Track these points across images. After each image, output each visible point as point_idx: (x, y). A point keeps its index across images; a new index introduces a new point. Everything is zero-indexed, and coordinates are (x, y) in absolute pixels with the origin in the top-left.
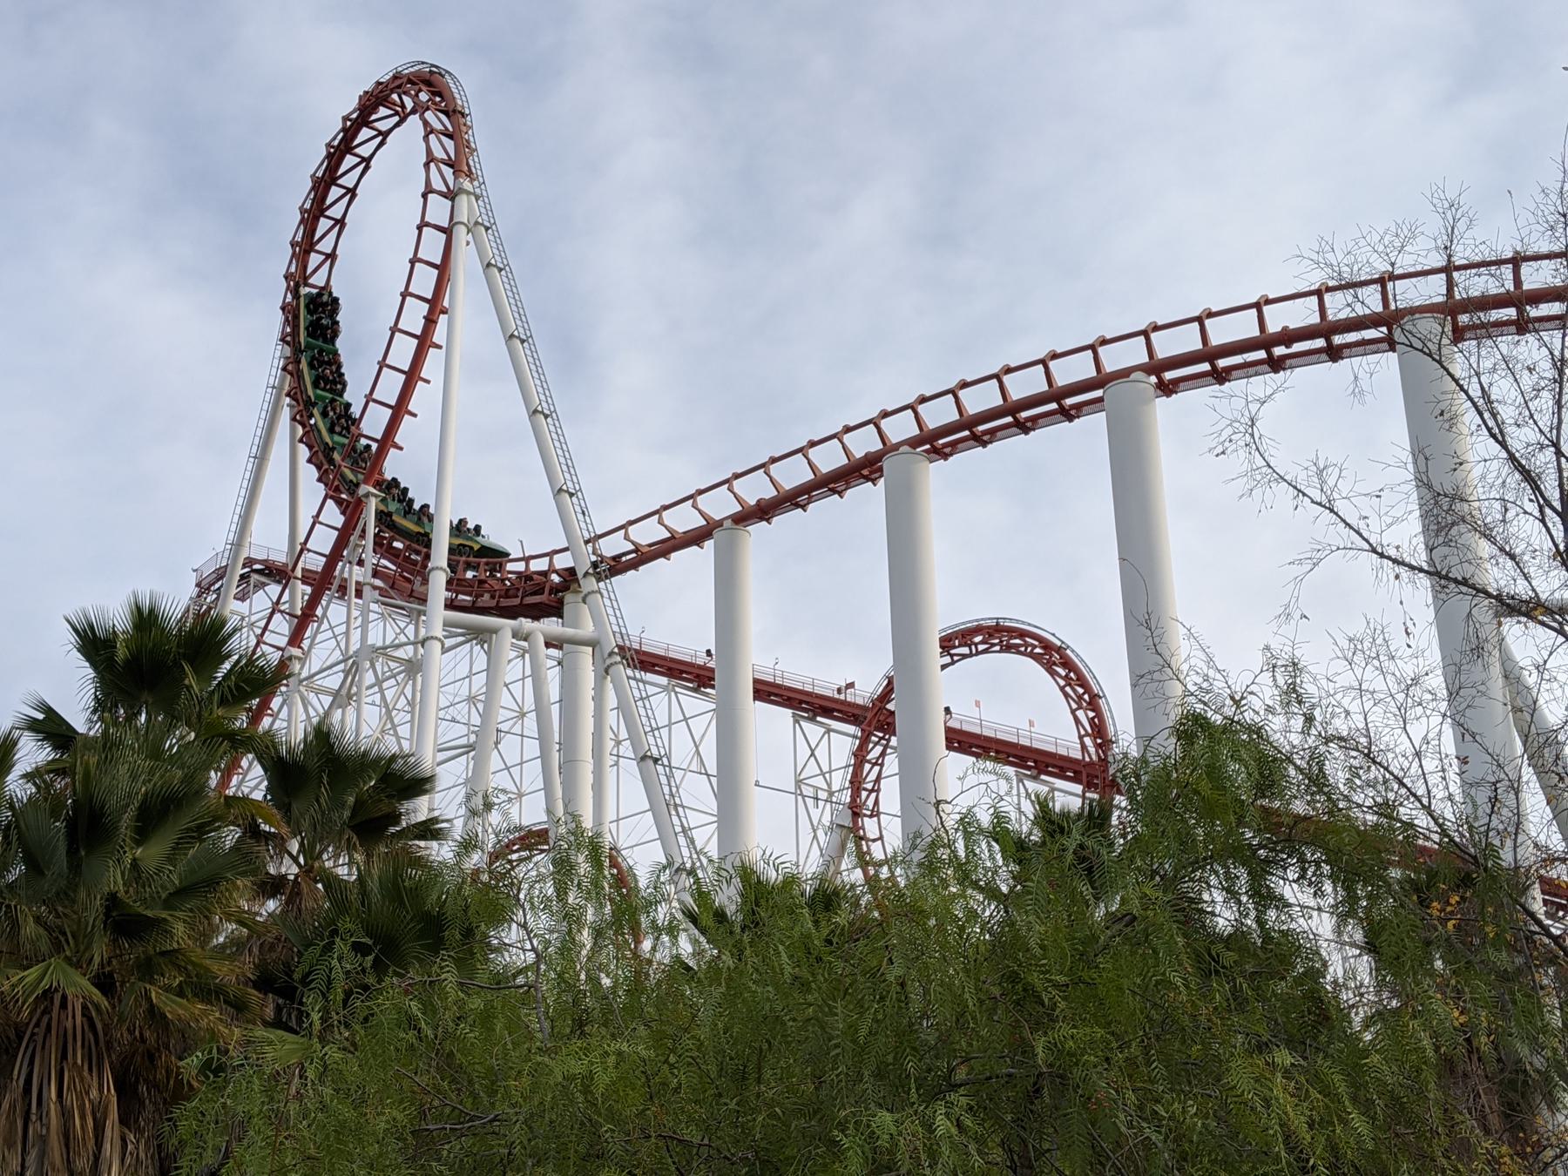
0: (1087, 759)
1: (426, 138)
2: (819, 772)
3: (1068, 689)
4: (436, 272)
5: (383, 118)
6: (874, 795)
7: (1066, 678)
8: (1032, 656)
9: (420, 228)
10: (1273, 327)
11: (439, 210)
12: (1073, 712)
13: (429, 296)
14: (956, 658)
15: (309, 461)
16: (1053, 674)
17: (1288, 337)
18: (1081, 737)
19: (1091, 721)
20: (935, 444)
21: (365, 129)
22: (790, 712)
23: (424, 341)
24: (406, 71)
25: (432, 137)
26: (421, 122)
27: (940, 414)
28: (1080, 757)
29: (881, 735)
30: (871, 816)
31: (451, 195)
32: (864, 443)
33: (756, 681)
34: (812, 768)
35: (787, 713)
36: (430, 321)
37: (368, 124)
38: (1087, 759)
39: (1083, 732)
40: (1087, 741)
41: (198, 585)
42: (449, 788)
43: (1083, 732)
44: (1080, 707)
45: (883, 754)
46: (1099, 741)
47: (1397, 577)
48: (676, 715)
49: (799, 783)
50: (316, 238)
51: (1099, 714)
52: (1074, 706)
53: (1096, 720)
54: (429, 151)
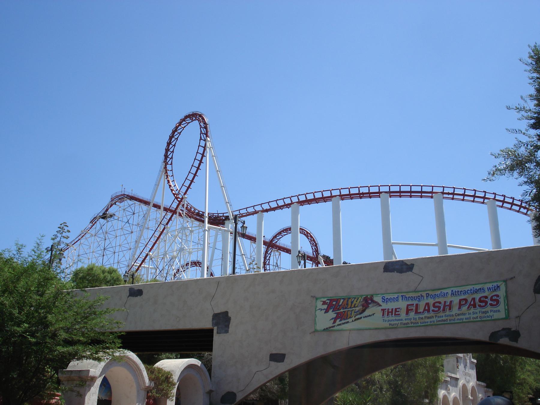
0: (314, 257)
1: (200, 129)
3: (311, 242)
5: (188, 120)
6: (269, 260)
7: (311, 239)
8: (304, 234)
9: (199, 146)
10: (361, 192)
11: (203, 143)
12: (312, 247)
14: (288, 233)
16: (308, 238)
17: (363, 194)
18: (313, 252)
19: (315, 249)
20: (301, 203)
21: (184, 122)
22: (250, 241)
23: (198, 168)
26: (199, 125)
27: (302, 198)
29: (271, 248)
30: (268, 265)
31: (205, 140)
32: (288, 201)
33: (164, 207)
34: (277, 256)
35: (249, 241)
36: (200, 165)
37: (185, 121)
38: (314, 257)
39: (313, 251)
40: (314, 253)
41: (111, 199)
43: (313, 251)
44: (313, 246)
45: (271, 252)
46: (316, 253)
48: (125, 215)
49: (251, 257)
50: (171, 142)
51: (317, 248)
52: (312, 245)
54: (201, 131)
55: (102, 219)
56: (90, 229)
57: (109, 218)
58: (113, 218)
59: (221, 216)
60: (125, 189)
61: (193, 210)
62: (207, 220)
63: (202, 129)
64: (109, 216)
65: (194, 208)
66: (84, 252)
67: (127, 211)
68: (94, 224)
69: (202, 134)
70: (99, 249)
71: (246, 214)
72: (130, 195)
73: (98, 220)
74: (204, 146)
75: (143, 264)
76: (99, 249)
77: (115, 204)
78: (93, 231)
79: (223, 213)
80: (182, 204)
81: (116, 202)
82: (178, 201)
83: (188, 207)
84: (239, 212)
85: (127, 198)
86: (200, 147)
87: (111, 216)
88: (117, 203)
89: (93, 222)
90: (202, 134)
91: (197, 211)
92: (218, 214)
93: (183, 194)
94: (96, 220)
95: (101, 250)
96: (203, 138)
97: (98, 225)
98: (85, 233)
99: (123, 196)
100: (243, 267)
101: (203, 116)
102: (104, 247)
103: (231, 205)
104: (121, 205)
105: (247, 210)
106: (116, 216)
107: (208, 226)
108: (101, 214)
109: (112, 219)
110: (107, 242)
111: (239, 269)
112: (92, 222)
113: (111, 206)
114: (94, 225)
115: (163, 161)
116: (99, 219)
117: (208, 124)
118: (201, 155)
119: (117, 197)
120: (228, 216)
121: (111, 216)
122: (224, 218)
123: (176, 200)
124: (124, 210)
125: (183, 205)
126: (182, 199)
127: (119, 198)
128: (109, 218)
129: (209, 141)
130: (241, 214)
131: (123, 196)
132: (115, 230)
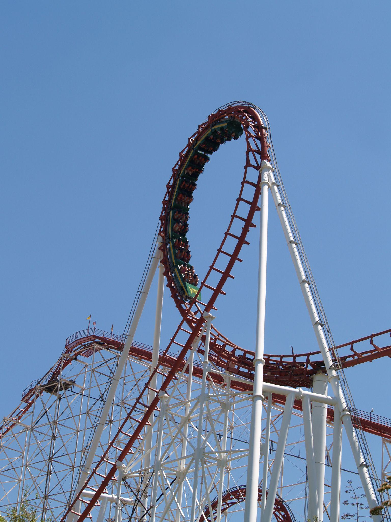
2: (54, 472)
4: (250, 206)
9: (243, 184)
11: (252, 175)
13: (246, 218)
15: (167, 286)
19: (283, 516)
22: (380, 438)
24: (233, 106)
25: (250, 140)
28: (195, 463)
31: (258, 168)
36: (245, 230)
42: (67, 418)
47: (10, 509)
53: (285, 516)
55: (47, 391)
56: (24, 412)
57: (63, 391)
58: (70, 389)
59: (302, 364)
60: (94, 324)
61: (229, 349)
62: (260, 369)
63: (250, 140)
64: (61, 387)
65: (231, 345)
66: (10, 465)
67: (101, 374)
68: (31, 404)
69: (250, 153)
70: (40, 458)
71: (370, 354)
72: (108, 337)
73: (38, 396)
74: (256, 182)
75: (107, 490)
76: (40, 458)
77: (76, 359)
78: (27, 420)
79: (229, 103)
80: (201, 336)
81: (76, 355)
82: (192, 327)
83: (218, 342)
84: (352, 349)
85: (101, 345)
86: (246, 185)
87: (66, 386)
88: (79, 357)
89: (29, 398)
90: (250, 153)
91: (242, 353)
92: (294, 357)
93: (202, 308)
94: (34, 396)
95: (45, 461)
96: (253, 162)
97: (38, 407)
98: (12, 422)
99: (92, 341)
100: (364, 500)
101: (255, 111)
102: (49, 455)
103: (328, 331)
104: (88, 360)
105: (372, 342)
106: (78, 386)
107: (264, 386)
108: (45, 382)
109: (68, 393)
110: (58, 442)
111: (353, 504)
112: (27, 398)
113: (65, 365)
114: (30, 406)
115: (158, 232)
116: (41, 393)
117: (266, 129)
118: (250, 206)
119: (79, 342)
120: (322, 363)
121: (66, 386)
122: (310, 368)
123: (185, 326)
124: (93, 371)
125: (204, 339)
126: (202, 320)
127: (84, 345)
128: (61, 390)
129: (268, 169)
130: (356, 354)
131: (92, 341)
132: (73, 417)
